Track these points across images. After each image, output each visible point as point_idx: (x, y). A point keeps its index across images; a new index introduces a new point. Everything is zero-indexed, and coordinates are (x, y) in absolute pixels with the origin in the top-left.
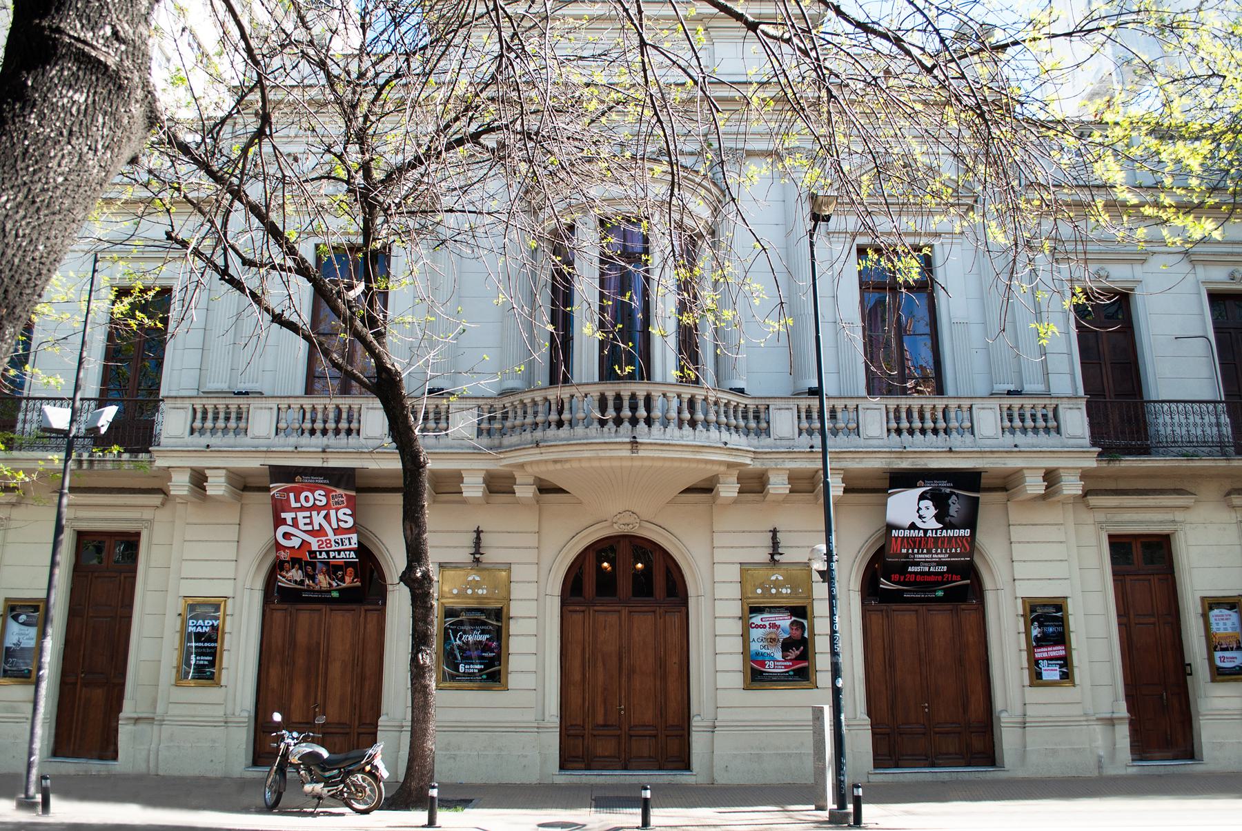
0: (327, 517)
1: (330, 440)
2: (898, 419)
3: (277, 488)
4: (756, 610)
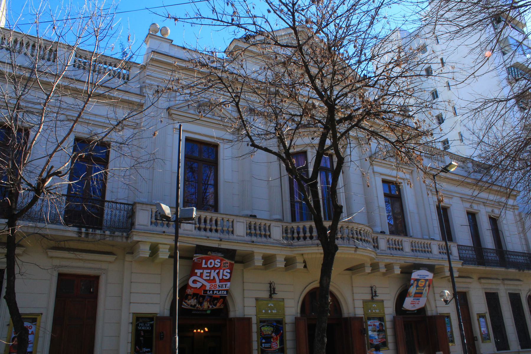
0: (218, 274)
3: (196, 257)
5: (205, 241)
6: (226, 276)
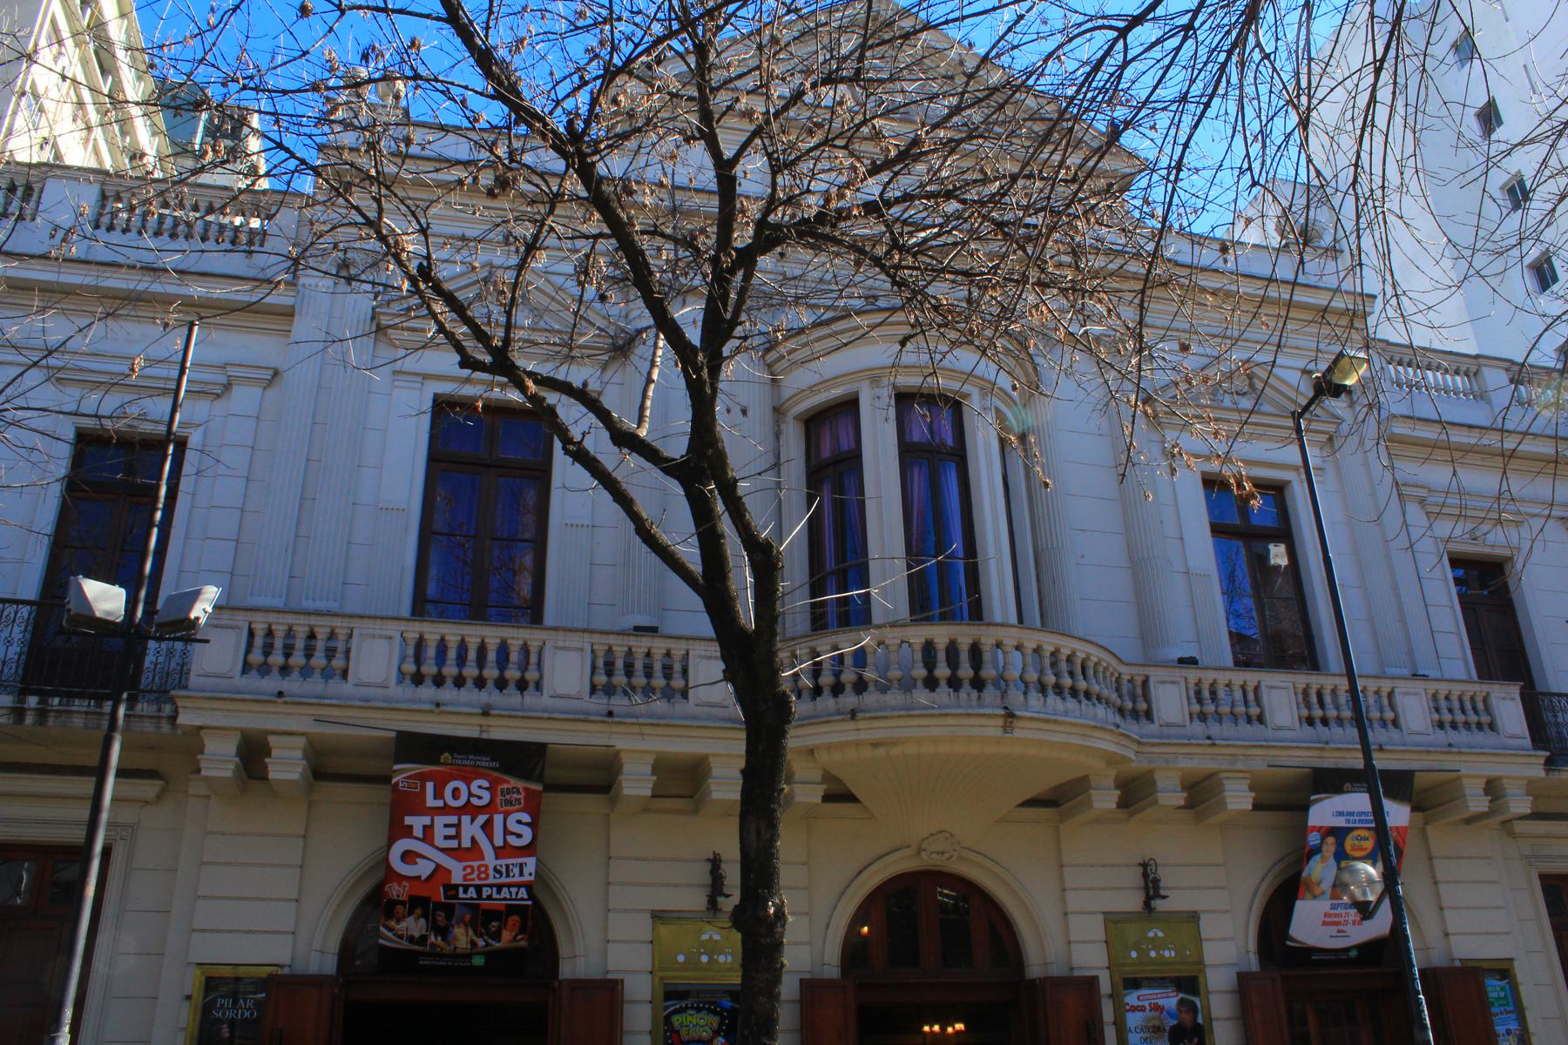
0: (487, 828)
1: (489, 696)
2: (418, 660)
3: (403, 773)
4: (1133, 984)
5: (430, 718)
6: (519, 836)
